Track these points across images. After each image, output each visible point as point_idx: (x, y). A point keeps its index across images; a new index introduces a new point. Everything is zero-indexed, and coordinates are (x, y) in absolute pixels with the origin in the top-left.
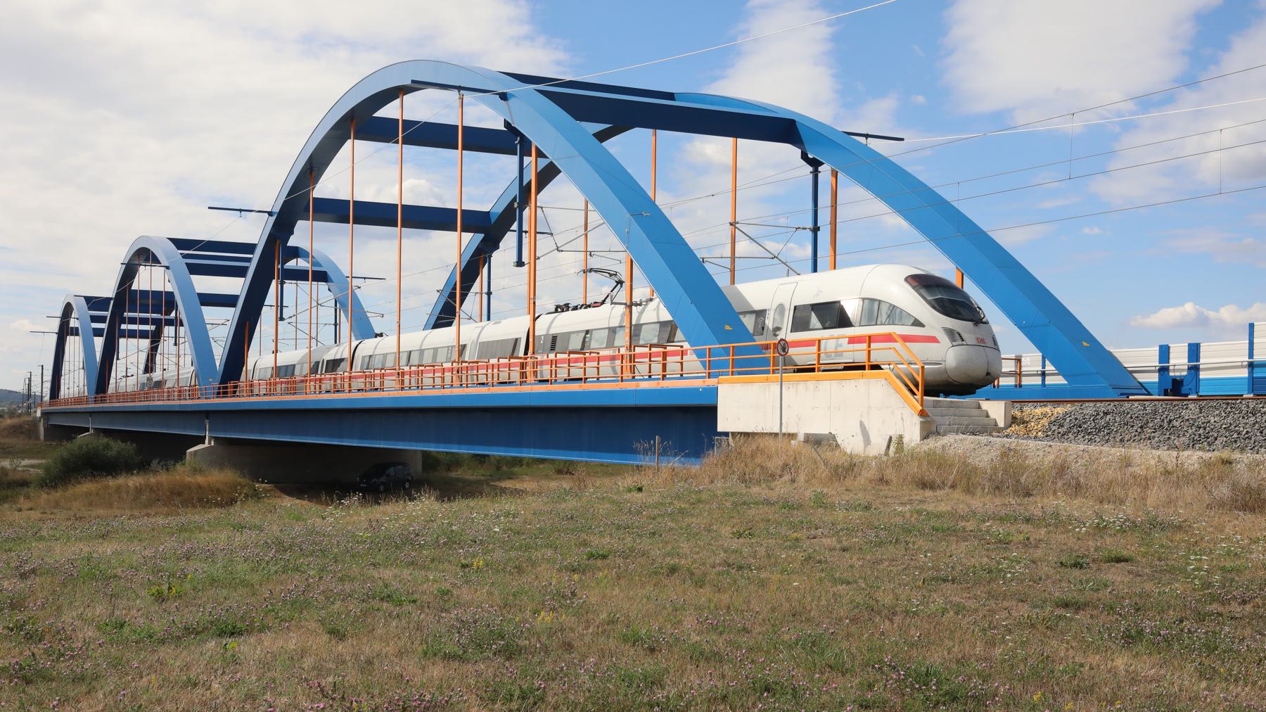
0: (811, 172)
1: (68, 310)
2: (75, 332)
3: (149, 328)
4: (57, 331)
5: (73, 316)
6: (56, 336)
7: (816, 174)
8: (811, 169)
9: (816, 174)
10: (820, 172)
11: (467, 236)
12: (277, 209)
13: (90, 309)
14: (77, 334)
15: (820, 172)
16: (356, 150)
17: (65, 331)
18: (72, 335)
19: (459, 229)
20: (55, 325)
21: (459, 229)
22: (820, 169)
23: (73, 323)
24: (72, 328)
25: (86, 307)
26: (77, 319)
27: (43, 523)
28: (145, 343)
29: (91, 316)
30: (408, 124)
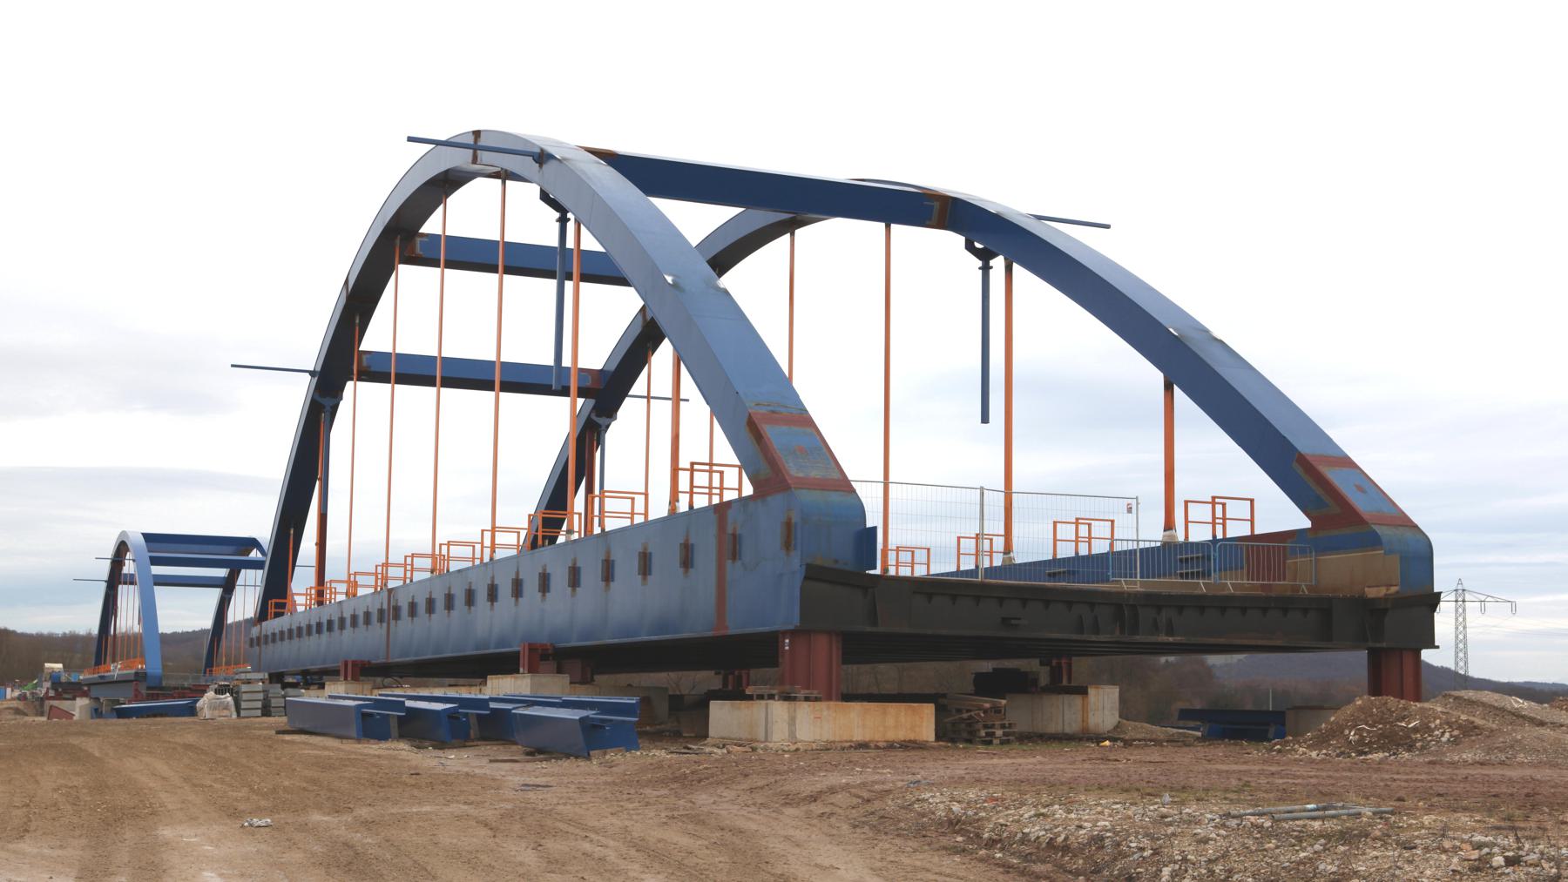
0: (980, 268)
1: (122, 549)
2: (131, 581)
3: (222, 573)
4: (106, 578)
5: (127, 557)
6: (104, 585)
7: (986, 269)
8: (980, 263)
9: (986, 269)
10: (992, 267)
11: (580, 401)
12: (318, 369)
13: (149, 551)
14: (132, 583)
15: (992, 267)
16: (410, 281)
17: (116, 578)
18: (125, 583)
19: (355, 378)
20: (104, 569)
21: (355, 378)
22: (992, 263)
23: (129, 568)
24: (126, 575)
25: (146, 550)
26: (134, 561)
27: (107, 838)
28: (216, 593)
29: (150, 557)
30: (454, 241)
